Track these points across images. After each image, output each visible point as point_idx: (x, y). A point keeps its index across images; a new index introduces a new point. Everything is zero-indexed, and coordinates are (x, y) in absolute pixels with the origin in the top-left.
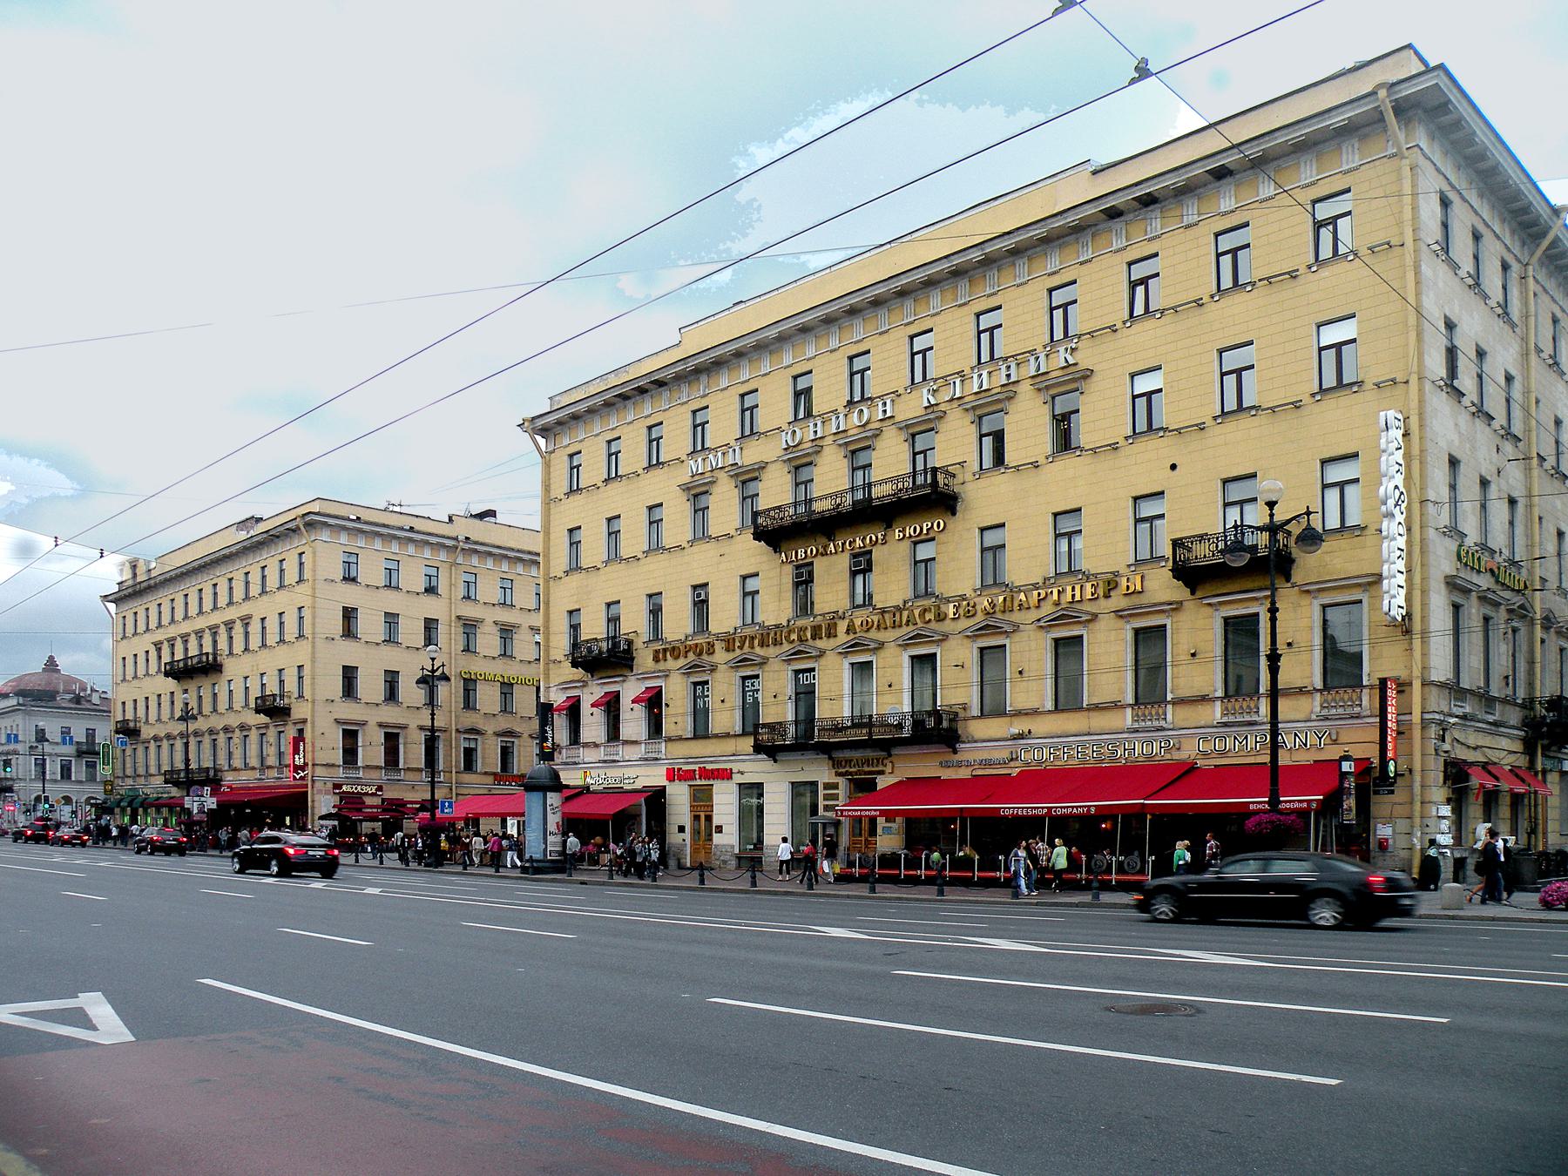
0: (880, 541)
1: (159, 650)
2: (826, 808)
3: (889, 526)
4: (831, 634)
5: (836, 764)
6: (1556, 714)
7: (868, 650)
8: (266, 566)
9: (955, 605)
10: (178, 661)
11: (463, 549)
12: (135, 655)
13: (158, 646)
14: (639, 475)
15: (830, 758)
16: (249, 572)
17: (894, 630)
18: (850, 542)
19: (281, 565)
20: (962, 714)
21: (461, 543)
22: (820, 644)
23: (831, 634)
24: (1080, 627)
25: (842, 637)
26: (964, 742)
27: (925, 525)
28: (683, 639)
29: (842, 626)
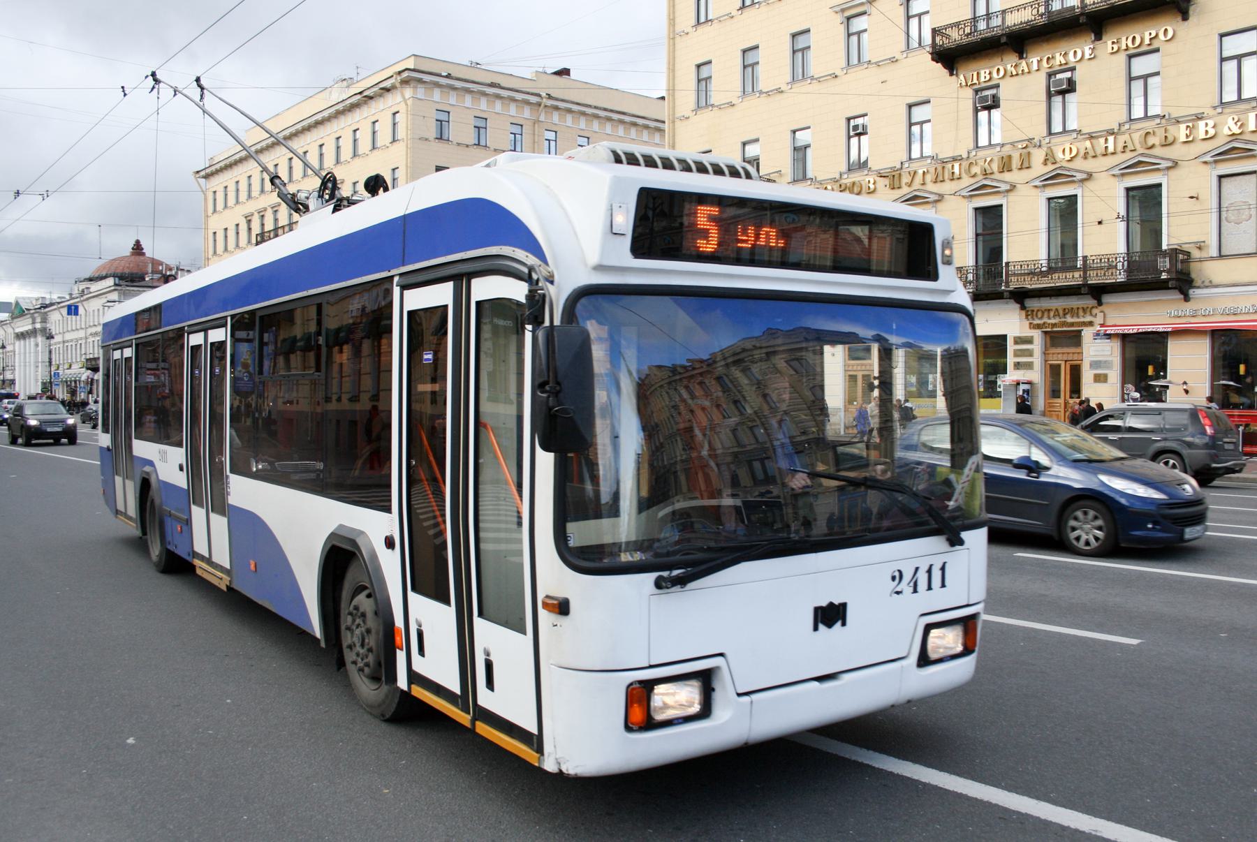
0: (1087, 56)
1: (249, 222)
2: (1018, 366)
3: (1099, 37)
4: (1025, 165)
5: (1030, 314)
6: (246, 321)
7: (1158, 170)
8: (358, 129)
9: (1188, 127)
10: (270, 232)
11: (546, 106)
12: (226, 229)
13: (249, 218)
14: (732, 17)
15: (1023, 308)
16: (323, 145)
17: (934, 185)
18: (1048, 58)
19: (355, 135)
20: (1196, 254)
21: (544, 100)
22: (1007, 176)
23: (1025, 165)
24: (1076, 185)
25: (1039, 168)
26: (1199, 287)
27: (1147, 34)
28: (838, 176)
29: (1038, 156)
